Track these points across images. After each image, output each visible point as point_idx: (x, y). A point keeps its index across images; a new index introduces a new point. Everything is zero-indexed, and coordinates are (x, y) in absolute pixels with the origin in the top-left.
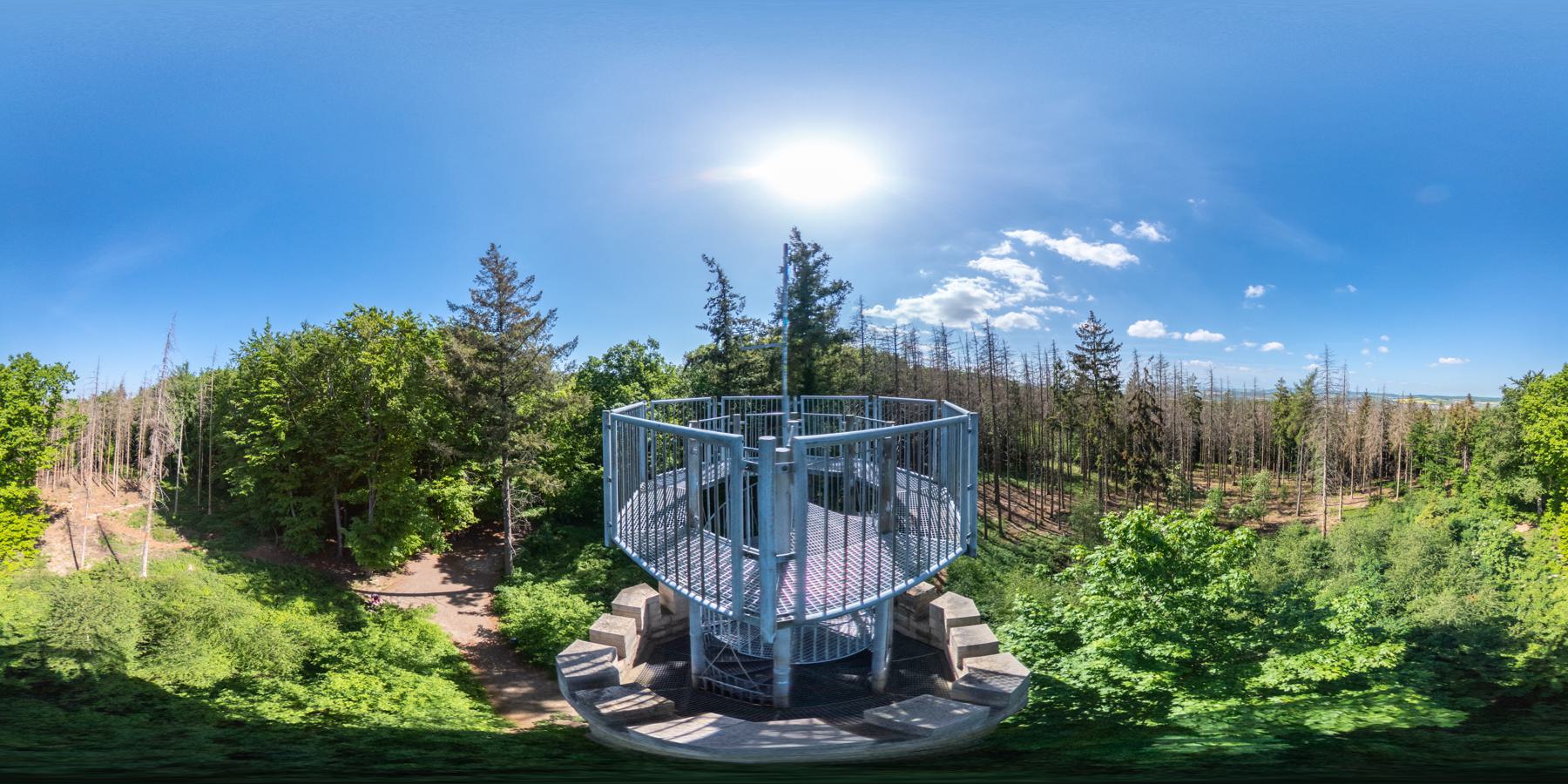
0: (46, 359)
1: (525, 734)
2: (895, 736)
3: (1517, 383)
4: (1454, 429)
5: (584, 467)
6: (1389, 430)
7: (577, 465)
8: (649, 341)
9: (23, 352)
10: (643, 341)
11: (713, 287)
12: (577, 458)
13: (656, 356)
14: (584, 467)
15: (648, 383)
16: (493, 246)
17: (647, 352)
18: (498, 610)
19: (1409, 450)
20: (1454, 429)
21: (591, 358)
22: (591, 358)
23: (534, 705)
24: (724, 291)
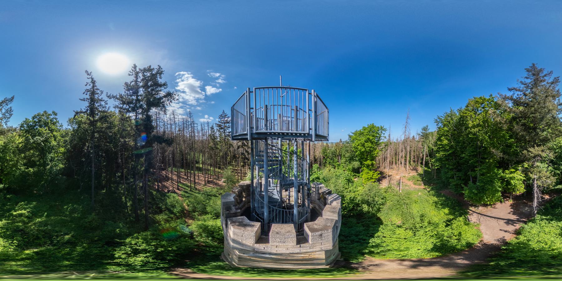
0: (378, 124)
1: (92, 270)
2: (425, 264)
3: (353, 133)
4: (336, 150)
5: (22, 168)
6: (316, 150)
7: (18, 167)
8: (53, 112)
9: (371, 123)
10: (50, 112)
11: (88, 84)
12: (19, 164)
13: (56, 119)
14: (22, 168)
15: (52, 130)
16: (534, 65)
17: (52, 117)
18: (518, 233)
19: (322, 158)
20: (336, 150)
21: (26, 119)
22: (26, 119)
23: (100, 262)
24: (93, 87)
